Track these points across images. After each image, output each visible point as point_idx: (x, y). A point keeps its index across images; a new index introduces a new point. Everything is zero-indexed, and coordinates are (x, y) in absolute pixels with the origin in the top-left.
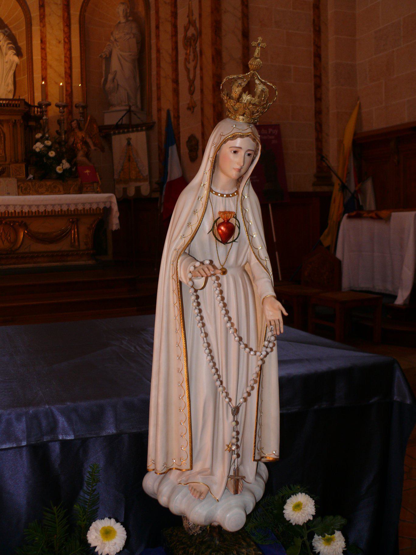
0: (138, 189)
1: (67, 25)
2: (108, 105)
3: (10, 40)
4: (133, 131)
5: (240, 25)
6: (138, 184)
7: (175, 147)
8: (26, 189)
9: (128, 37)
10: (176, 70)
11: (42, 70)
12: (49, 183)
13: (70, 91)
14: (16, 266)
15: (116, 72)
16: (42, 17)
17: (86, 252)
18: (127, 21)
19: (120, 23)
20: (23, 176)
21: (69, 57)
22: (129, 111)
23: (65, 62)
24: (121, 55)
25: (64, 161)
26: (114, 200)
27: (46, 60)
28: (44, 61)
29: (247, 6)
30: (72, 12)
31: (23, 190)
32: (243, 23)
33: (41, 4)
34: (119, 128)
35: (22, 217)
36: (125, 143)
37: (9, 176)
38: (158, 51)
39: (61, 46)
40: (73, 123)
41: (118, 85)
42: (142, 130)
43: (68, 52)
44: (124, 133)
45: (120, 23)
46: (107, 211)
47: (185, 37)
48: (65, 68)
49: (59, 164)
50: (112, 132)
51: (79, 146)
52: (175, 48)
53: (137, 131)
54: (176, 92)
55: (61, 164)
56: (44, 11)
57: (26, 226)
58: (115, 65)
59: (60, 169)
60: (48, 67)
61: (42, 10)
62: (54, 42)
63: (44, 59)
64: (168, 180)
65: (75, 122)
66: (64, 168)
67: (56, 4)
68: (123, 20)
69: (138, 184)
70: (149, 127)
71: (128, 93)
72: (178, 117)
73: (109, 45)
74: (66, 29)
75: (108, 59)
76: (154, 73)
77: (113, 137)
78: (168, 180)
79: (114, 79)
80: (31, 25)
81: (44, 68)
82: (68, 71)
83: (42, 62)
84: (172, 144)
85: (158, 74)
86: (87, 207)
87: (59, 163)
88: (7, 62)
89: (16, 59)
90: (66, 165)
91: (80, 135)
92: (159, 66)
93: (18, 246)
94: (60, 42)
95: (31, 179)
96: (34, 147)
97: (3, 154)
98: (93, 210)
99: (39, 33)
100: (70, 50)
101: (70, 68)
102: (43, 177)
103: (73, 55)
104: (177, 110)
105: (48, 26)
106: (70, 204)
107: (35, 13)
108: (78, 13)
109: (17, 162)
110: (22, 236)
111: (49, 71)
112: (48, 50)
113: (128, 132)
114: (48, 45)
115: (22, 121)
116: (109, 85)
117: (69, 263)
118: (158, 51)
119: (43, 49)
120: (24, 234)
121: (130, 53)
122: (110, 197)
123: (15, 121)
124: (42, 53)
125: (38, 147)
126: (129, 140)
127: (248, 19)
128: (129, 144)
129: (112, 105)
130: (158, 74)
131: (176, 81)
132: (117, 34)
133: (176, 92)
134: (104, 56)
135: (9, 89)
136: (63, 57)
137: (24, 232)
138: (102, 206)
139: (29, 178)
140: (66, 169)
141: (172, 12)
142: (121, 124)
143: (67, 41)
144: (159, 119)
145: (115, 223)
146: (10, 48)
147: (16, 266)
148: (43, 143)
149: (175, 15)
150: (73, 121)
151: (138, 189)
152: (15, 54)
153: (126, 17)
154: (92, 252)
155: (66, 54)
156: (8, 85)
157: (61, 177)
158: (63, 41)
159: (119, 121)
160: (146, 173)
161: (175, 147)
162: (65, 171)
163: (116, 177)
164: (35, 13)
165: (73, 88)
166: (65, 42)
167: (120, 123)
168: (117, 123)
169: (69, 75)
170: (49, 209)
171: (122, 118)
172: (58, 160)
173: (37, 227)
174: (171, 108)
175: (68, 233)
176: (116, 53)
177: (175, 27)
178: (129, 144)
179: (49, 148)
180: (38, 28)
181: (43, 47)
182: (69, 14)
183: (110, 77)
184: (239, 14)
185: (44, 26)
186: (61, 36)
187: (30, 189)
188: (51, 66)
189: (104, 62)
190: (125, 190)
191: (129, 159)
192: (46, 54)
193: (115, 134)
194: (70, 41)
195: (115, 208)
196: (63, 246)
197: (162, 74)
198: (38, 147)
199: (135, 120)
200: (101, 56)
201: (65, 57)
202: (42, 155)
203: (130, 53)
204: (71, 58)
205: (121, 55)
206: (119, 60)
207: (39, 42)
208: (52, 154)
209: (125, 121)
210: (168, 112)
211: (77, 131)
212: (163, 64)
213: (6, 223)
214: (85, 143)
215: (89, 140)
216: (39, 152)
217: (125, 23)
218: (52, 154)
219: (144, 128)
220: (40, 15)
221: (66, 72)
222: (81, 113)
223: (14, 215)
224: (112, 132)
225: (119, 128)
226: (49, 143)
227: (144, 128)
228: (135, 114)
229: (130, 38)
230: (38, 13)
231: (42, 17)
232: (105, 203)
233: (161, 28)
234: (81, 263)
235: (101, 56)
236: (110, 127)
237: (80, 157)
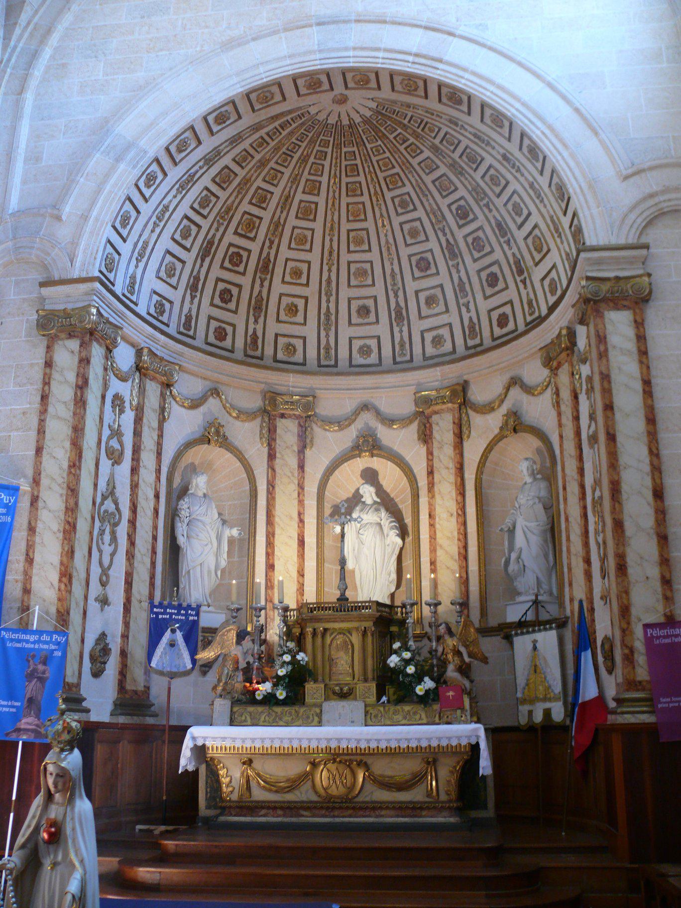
0: (547, 713)
1: (460, 493)
2: (513, 593)
3: (395, 518)
4: (540, 631)
5: (648, 482)
6: (547, 705)
7: (589, 652)
8: (376, 716)
9: (531, 503)
10: (586, 544)
11: (431, 552)
12: (407, 708)
13: (465, 576)
14: (351, 820)
15: (521, 550)
16: (431, 485)
17: (447, 805)
18: (535, 479)
19: (525, 483)
20: (372, 699)
21: (463, 533)
22: (536, 602)
23: (459, 540)
24: (526, 526)
25: (426, 679)
26: (482, 733)
27: (435, 539)
28: (433, 540)
29: (658, 456)
30: (466, 476)
31: (369, 719)
32: (653, 479)
33: (429, 470)
34: (523, 626)
35: (348, 754)
36: (530, 646)
37: (355, 699)
38: (567, 519)
39: (454, 520)
40: (441, 628)
41: (524, 566)
42: (551, 628)
43: (462, 528)
44: (528, 632)
45: (525, 483)
46: (475, 748)
47: (593, 498)
48: (459, 548)
49: (419, 683)
50: (513, 632)
51: (450, 657)
52: (585, 516)
53: (545, 629)
54: (588, 575)
55: (423, 683)
56: (433, 479)
57: (367, 767)
58: (520, 540)
59: (420, 690)
60: (438, 548)
61: (431, 478)
62: (445, 515)
63: (433, 538)
64: (580, 701)
65: (443, 626)
66: (427, 688)
67: (448, 468)
68: (529, 480)
69: (547, 705)
70: (561, 624)
71: (537, 578)
72: (592, 610)
73: (513, 514)
74: (459, 498)
75: (512, 531)
76: (564, 549)
77: (515, 639)
78: (580, 701)
79: (519, 557)
80: (418, 497)
81: (433, 550)
82: (462, 551)
83: (430, 542)
84: (586, 649)
85: (568, 551)
86: (444, 743)
87: (420, 681)
88: (388, 545)
89: (399, 541)
90: (428, 684)
91: (451, 642)
92: (568, 539)
93: (357, 792)
94: (452, 515)
95: (384, 702)
96: (388, 662)
97: (351, 671)
98: (452, 746)
99: (427, 506)
100: (465, 524)
101: (465, 547)
102: (400, 700)
103: (469, 530)
104: (591, 601)
105: (437, 496)
106: (421, 739)
107: (423, 483)
108: (474, 476)
109: (366, 680)
110: (361, 780)
111: (440, 552)
112: (437, 526)
113: (534, 631)
114: (437, 519)
115: (373, 629)
116: (513, 567)
117: (420, 820)
118: (567, 519)
119: (432, 525)
120: (364, 777)
121: (538, 523)
122: (476, 730)
123: (365, 628)
124: (430, 530)
125: (393, 661)
126: (535, 642)
127: (660, 473)
128: (535, 648)
129: (519, 594)
130: (568, 551)
131: (588, 561)
132: (522, 499)
133: (588, 575)
134: (506, 529)
135: (391, 579)
136: (456, 534)
137: (364, 774)
138: (464, 742)
139: (382, 701)
140: (429, 689)
141: (578, 468)
142: (525, 621)
143: (460, 512)
144: (572, 612)
145: (485, 765)
146: (392, 528)
147: (351, 820)
148: (400, 656)
149: (581, 471)
150: (441, 625)
151: (547, 713)
152: (398, 535)
153: (533, 474)
154: (455, 805)
155: (459, 529)
156: (390, 575)
157: (425, 700)
158: (455, 513)
159: (522, 617)
160: (558, 688)
161: (589, 652)
162: (427, 692)
163: (519, 695)
164: (423, 483)
165: (470, 572)
166: (458, 515)
167: (523, 619)
168: (520, 620)
169: (464, 557)
170: (394, 745)
171: (526, 613)
172: (418, 678)
173: (381, 768)
174: (583, 597)
175: (422, 777)
176: (521, 523)
177: (582, 487)
178: (535, 648)
179: (407, 662)
180: (427, 499)
181: (432, 523)
182: (463, 479)
183: (514, 556)
184: (647, 468)
185: (433, 497)
186: (453, 507)
187: (382, 716)
188: (441, 546)
189: (506, 536)
190: (530, 713)
191: (536, 669)
192: (435, 532)
193: (517, 635)
194: (464, 513)
195: (483, 745)
196: (416, 795)
197: (572, 549)
198: (393, 661)
199: (544, 616)
200: (501, 530)
201: (458, 533)
202: (398, 671)
203: (538, 523)
204: (465, 535)
205: (526, 526)
206: (524, 532)
207: (428, 516)
208: (411, 670)
209: (530, 617)
210: (581, 602)
211: (447, 637)
212: (572, 537)
213: (340, 762)
214: (458, 653)
215: (462, 649)
216: (394, 668)
217: (531, 483)
218: (411, 670)
219: (554, 625)
220: (429, 484)
221: (459, 553)
222: (458, 612)
223: (354, 751)
224: (513, 632)
225: (523, 626)
226: (407, 655)
227: (554, 625)
228: (543, 606)
229: (535, 503)
230: (426, 482)
231: (431, 486)
232: (469, 737)
233: (568, 489)
234: (440, 820)
235: (501, 530)
236: (511, 626)
237: (451, 672)
